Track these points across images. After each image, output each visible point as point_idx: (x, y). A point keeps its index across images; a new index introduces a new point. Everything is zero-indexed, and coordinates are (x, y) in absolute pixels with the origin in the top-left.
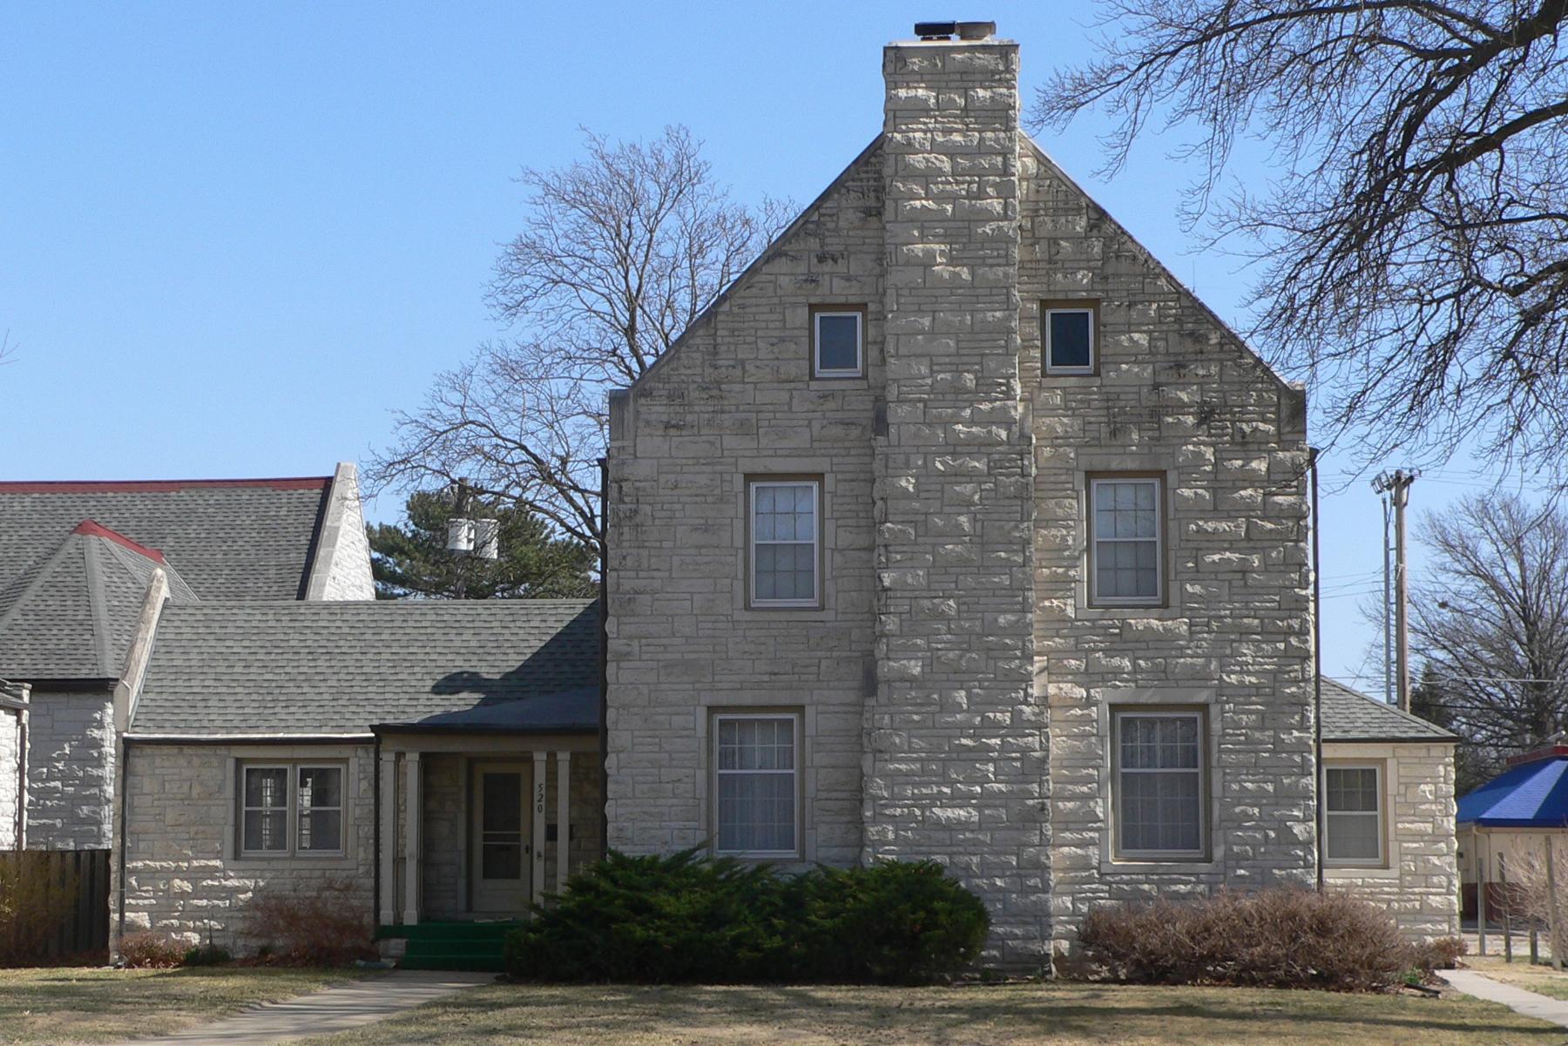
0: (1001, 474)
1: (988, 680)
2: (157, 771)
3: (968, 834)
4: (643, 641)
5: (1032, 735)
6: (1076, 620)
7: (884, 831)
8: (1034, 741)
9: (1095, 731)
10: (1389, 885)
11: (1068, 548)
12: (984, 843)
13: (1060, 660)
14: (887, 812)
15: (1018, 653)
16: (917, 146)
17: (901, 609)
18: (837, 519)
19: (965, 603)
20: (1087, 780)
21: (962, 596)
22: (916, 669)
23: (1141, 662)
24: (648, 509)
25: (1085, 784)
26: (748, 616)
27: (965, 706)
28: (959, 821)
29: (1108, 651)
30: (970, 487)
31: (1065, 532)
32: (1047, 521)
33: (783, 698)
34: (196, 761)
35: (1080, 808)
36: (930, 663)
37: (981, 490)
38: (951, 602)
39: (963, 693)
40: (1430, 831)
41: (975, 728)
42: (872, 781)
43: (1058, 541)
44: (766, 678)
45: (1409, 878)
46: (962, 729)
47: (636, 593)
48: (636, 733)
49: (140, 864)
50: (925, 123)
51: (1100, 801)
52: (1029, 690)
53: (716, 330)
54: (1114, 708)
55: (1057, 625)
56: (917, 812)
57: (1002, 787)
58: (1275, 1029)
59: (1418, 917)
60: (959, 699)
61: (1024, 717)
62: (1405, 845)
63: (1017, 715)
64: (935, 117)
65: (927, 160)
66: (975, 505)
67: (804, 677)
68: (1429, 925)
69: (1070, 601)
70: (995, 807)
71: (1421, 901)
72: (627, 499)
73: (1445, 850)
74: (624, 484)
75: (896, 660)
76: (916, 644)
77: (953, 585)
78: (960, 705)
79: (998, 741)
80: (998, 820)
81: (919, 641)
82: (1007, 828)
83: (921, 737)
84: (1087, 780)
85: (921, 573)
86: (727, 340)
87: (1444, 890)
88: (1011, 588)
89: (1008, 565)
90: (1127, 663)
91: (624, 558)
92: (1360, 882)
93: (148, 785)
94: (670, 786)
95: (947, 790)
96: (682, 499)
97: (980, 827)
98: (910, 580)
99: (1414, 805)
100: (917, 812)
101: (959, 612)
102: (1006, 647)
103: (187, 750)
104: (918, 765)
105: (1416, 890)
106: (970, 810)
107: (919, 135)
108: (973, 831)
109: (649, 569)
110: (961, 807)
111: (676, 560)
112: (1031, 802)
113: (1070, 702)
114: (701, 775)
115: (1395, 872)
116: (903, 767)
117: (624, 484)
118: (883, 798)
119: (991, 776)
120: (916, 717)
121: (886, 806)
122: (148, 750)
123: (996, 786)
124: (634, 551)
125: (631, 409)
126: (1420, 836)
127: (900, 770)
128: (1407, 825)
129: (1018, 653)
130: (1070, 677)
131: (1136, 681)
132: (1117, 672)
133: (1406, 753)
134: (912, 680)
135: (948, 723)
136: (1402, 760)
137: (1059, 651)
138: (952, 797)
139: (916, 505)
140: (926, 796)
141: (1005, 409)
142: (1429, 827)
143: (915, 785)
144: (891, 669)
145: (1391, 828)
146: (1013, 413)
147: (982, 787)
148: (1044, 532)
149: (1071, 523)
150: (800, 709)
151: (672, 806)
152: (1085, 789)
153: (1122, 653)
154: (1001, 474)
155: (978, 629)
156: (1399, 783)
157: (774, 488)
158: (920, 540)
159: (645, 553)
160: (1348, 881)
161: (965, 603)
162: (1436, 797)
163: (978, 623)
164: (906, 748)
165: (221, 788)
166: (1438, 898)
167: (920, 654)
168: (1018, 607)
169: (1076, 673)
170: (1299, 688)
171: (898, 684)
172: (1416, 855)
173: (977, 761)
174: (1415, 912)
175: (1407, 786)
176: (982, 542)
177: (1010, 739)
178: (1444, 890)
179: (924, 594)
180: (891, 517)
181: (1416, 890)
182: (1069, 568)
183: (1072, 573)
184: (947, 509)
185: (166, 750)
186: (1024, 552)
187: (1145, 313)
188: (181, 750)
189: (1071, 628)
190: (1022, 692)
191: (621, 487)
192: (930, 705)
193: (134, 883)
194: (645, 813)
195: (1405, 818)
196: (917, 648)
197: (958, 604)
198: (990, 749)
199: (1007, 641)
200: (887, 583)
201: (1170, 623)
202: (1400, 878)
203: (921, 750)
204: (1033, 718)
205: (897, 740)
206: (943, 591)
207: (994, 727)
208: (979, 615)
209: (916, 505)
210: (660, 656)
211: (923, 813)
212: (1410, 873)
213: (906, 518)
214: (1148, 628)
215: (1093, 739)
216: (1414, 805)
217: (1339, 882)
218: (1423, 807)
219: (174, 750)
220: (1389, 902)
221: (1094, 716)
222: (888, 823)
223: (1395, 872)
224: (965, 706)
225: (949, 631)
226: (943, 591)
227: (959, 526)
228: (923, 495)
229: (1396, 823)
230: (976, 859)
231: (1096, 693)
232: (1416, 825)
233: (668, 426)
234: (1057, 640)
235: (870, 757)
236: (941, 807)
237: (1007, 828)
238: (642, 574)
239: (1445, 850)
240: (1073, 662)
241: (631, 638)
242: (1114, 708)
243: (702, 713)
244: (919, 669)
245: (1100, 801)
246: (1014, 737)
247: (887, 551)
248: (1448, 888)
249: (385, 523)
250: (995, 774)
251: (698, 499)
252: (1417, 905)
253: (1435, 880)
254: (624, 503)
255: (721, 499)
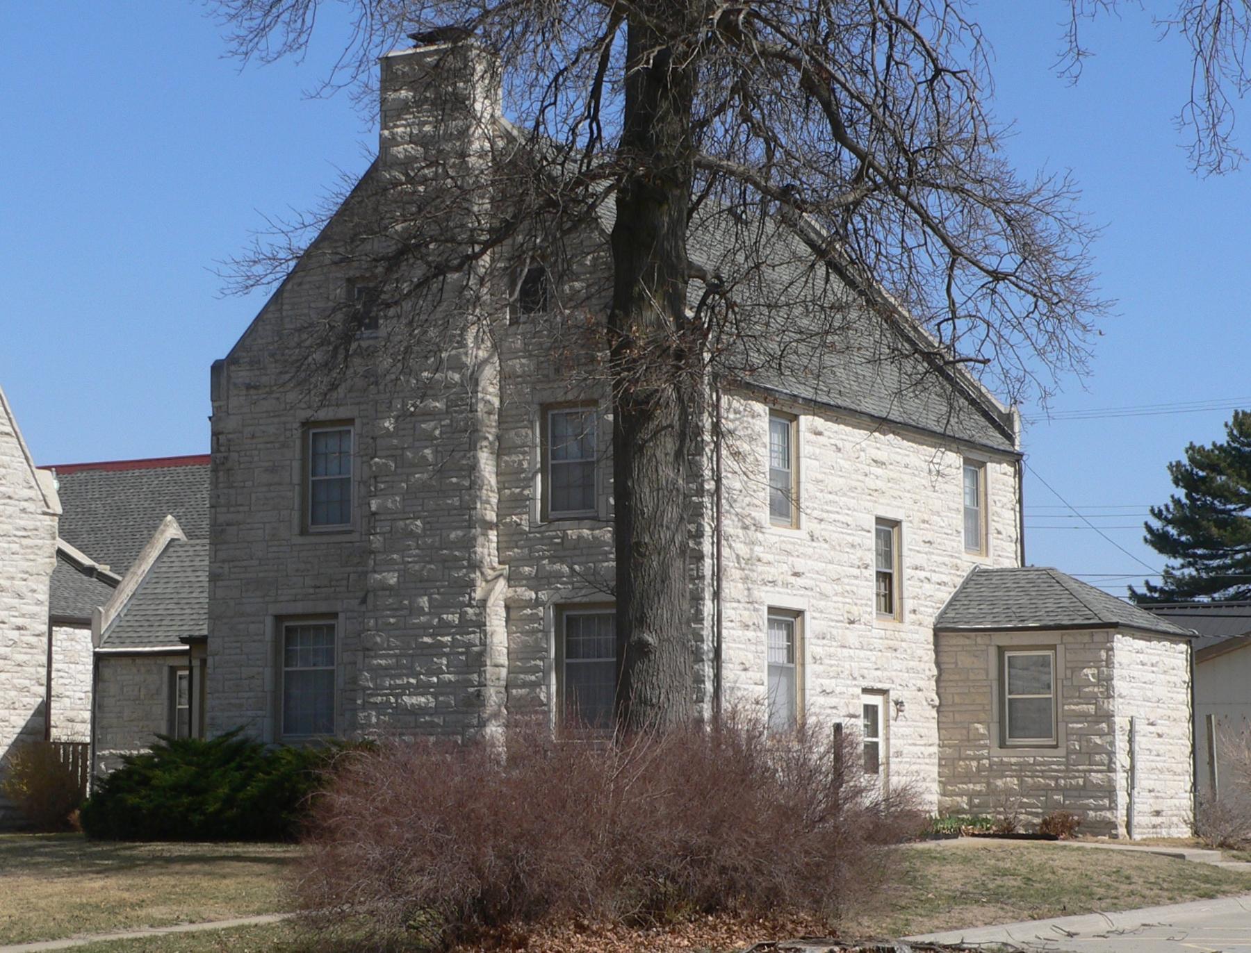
0: (456, 412)
1: (443, 587)
2: (119, 678)
3: (427, 718)
4: (231, 564)
5: (474, 632)
6: (530, 533)
7: (369, 716)
8: (475, 638)
9: (541, 628)
10: (1058, 763)
11: (524, 471)
12: (438, 725)
13: (518, 567)
14: (372, 700)
15: (465, 563)
16: (399, 139)
17: (384, 530)
18: (362, 456)
19: (428, 523)
20: (535, 670)
21: (427, 517)
22: (392, 579)
23: (577, 567)
24: (236, 455)
25: (534, 673)
26: (300, 540)
27: (426, 610)
28: (420, 707)
29: (554, 559)
30: (432, 424)
31: (521, 457)
32: (509, 448)
33: (322, 607)
34: (143, 670)
35: (528, 694)
36: (403, 574)
37: (442, 426)
38: (418, 523)
39: (426, 599)
40: (1093, 712)
41: (433, 627)
42: (362, 675)
43: (516, 465)
44: (312, 591)
45: (1074, 757)
46: (424, 628)
47: (228, 525)
48: (226, 639)
49: (106, 752)
50: (406, 120)
51: (544, 688)
52: (473, 594)
53: (282, 304)
54: (559, 608)
55: (515, 538)
56: (392, 699)
57: (452, 677)
58: (33, 861)
59: (1082, 793)
60: (422, 604)
61: (468, 617)
62: (1070, 725)
63: (463, 615)
64: (413, 113)
65: (406, 150)
66: (436, 438)
67: (338, 589)
68: (1092, 801)
69: (525, 517)
70: (447, 694)
71: (1085, 778)
72: (222, 449)
73: (1106, 730)
74: (220, 437)
75: (380, 573)
76: (393, 559)
77: (420, 508)
78: (423, 608)
79: (449, 638)
80: (448, 705)
81: (395, 556)
82: (455, 712)
83: (396, 637)
84: (535, 670)
85: (398, 499)
86: (290, 313)
87: (1105, 768)
88: (461, 507)
89: (458, 488)
90: (565, 569)
91: (219, 496)
92: (1031, 760)
93: (113, 689)
94: (247, 682)
95: (413, 681)
96: (259, 446)
97: (436, 711)
98: (390, 505)
99: (1079, 688)
100: (392, 699)
101: (424, 529)
102: (457, 559)
103: (139, 661)
104: (394, 660)
105: (1080, 768)
106: (429, 697)
107: (400, 130)
108: (431, 715)
109: (237, 505)
110: (422, 695)
111: (253, 496)
112: (471, 690)
113: (523, 604)
114: (268, 672)
115: (1061, 751)
116: (383, 662)
117: (220, 437)
118: (369, 688)
119: (444, 668)
120: (392, 620)
121: (372, 695)
122: (113, 662)
123: (447, 677)
124: (226, 491)
125: (225, 374)
126: (1082, 716)
127: (381, 665)
128: (1073, 707)
129: (465, 563)
130: (524, 582)
131: (572, 583)
132: (558, 576)
133: (1070, 639)
134: (390, 588)
135: (414, 624)
136: (1069, 646)
137: (518, 560)
138: (417, 686)
139: (395, 441)
140: (399, 686)
141: (458, 357)
142: (1091, 709)
143: (392, 677)
144: (375, 580)
145: (1060, 710)
146: (464, 359)
147: (438, 678)
148: (506, 458)
149: (526, 449)
150: (335, 615)
151: (249, 698)
152: (533, 678)
153: (562, 560)
154: (456, 412)
155: (437, 544)
156: (1066, 668)
157: (340, 432)
158: (399, 471)
159: (232, 491)
160: (1022, 760)
161: (428, 523)
162: (1099, 680)
163: (437, 539)
164: (385, 645)
165: (158, 692)
166: (1099, 775)
167: (396, 567)
168: (466, 524)
169: (528, 578)
170: (694, 584)
171: (380, 593)
172: (1082, 736)
173: (435, 655)
174: (1078, 788)
175: (1073, 670)
176: (441, 472)
177: (458, 637)
178: (1105, 768)
179: (401, 516)
180: (379, 453)
181: (1080, 768)
182: (524, 488)
183: (526, 492)
184: (417, 444)
185: (124, 661)
186: (470, 477)
187: (582, 264)
188: (134, 660)
189: (526, 539)
190: (467, 596)
191: (218, 439)
192: (402, 609)
193: (103, 767)
194: (230, 704)
195: (1070, 701)
196: (393, 562)
197: (424, 524)
198: (443, 645)
199: (457, 553)
200: (374, 508)
201: (597, 532)
202: (1067, 757)
203: (396, 648)
204: (474, 618)
205: (378, 639)
206: (414, 513)
207: (445, 627)
208: (438, 532)
209: (395, 441)
210: (242, 576)
211: (396, 701)
212: (1075, 752)
213: (389, 453)
214: (580, 537)
215: (540, 635)
216: (1079, 688)
217: (1013, 760)
218: (1087, 690)
219: (129, 661)
220: (1057, 779)
221: (541, 614)
222: (371, 709)
223: (1061, 751)
224: (426, 610)
225: (418, 547)
226: (414, 513)
227: (424, 457)
228: (401, 433)
229: (1064, 705)
230: (432, 739)
231: (543, 595)
232: (1080, 707)
233: (249, 387)
234: (516, 550)
235: (361, 654)
236: (409, 695)
237: (455, 712)
238: (232, 509)
239: (1106, 730)
240: (527, 569)
241: (223, 561)
242: (559, 608)
243: (269, 621)
244: (395, 579)
245: (544, 688)
246: (461, 635)
247: (376, 482)
248: (1109, 766)
249: (1197, 444)
250: (447, 666)
251: (269, 445)
252: (1081, 781)
253: (1097, 758)
254: (221, 452)
255: (284, 445)
